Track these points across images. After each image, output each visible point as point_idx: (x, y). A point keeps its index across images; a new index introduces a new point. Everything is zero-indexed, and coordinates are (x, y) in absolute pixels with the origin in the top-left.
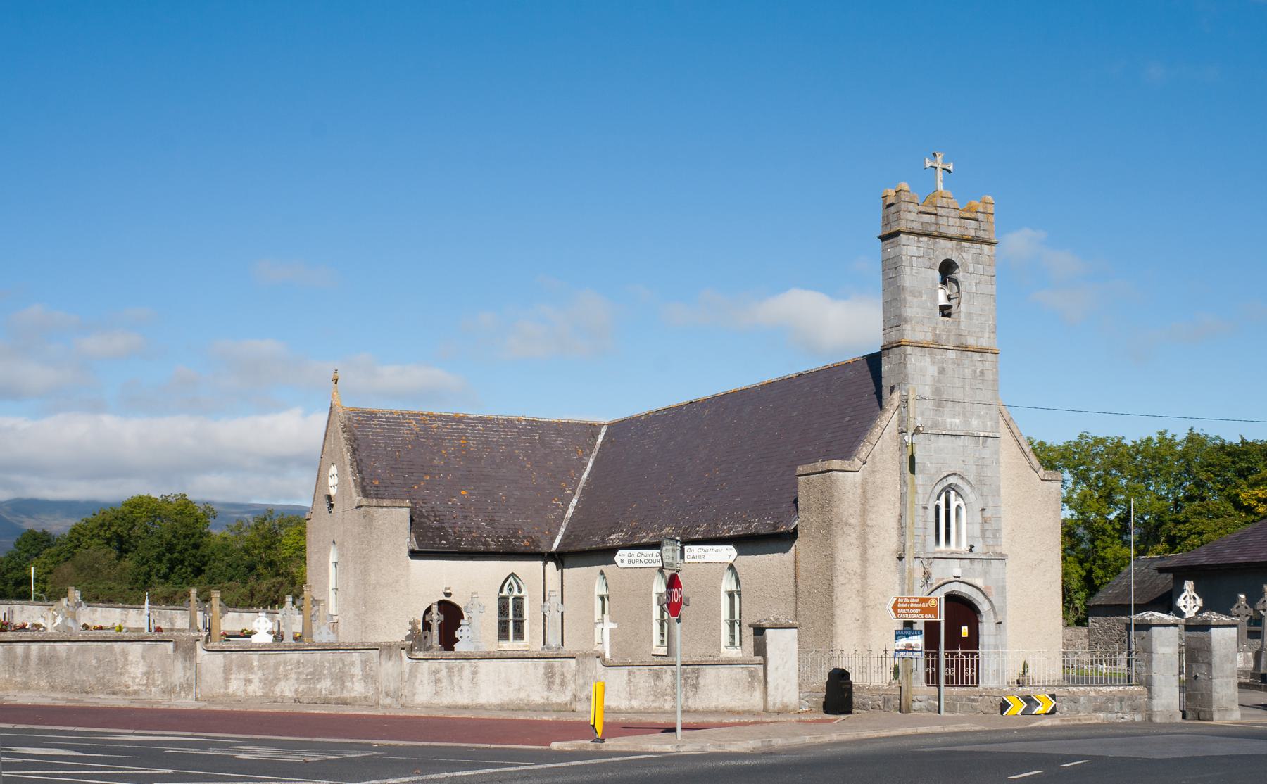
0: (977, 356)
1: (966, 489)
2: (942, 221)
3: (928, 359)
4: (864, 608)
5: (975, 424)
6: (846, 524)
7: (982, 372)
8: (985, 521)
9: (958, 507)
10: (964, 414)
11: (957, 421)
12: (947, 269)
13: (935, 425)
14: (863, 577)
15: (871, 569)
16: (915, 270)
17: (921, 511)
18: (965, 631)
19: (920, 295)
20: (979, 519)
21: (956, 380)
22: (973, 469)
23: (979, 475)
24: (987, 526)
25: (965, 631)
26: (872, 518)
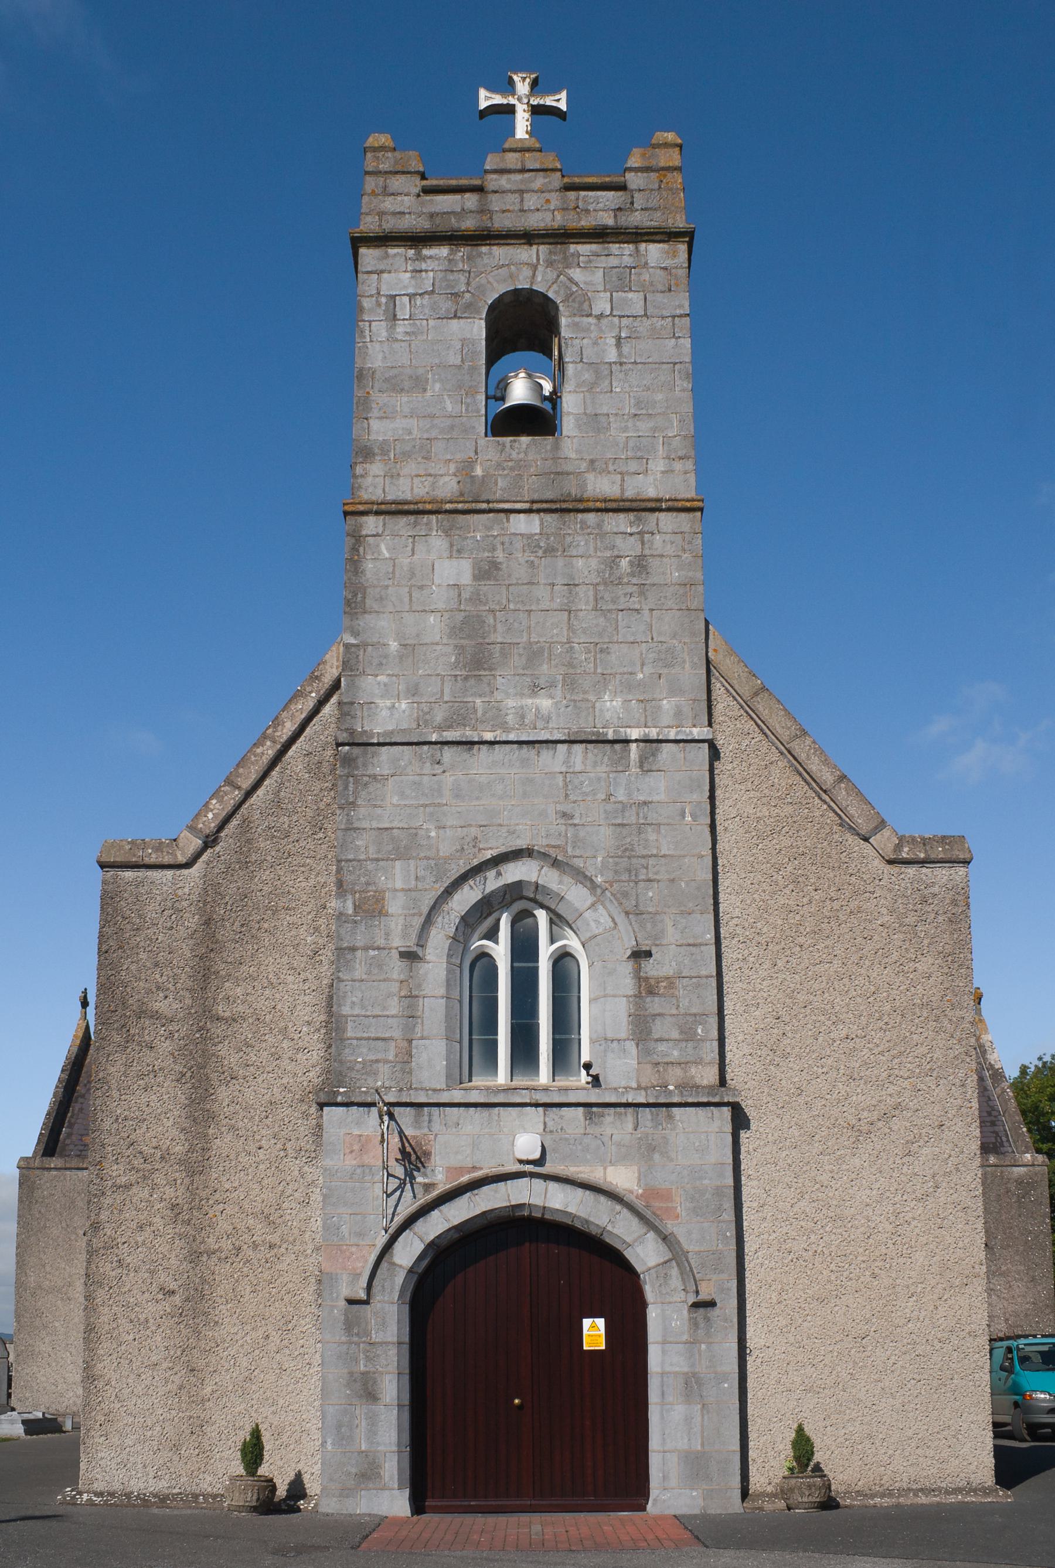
0: (620, 522)
1: (576, 896)
2: (496, 203)
3: (438, 542)
4: (195, 1256)
5: (611, 710)
6: (141, 1013)
7: (640, 564)
8: (646, 987)
9: (563, 960)
10: (570, 683)
11: (545, 703)
12: (523, 326)
13: (460, 717)
14: (196, 1164)
15: (223, 1144)
16: (401, 328)
17: (396, 968)
18: (594, 1332)
19: (419, 384)
20: (627, 984)
21: (541, 592)
22: (604, 836)
23: (627, 852)
24: (655, 1005)
25: (594, 1332)
26: (234, 995)
